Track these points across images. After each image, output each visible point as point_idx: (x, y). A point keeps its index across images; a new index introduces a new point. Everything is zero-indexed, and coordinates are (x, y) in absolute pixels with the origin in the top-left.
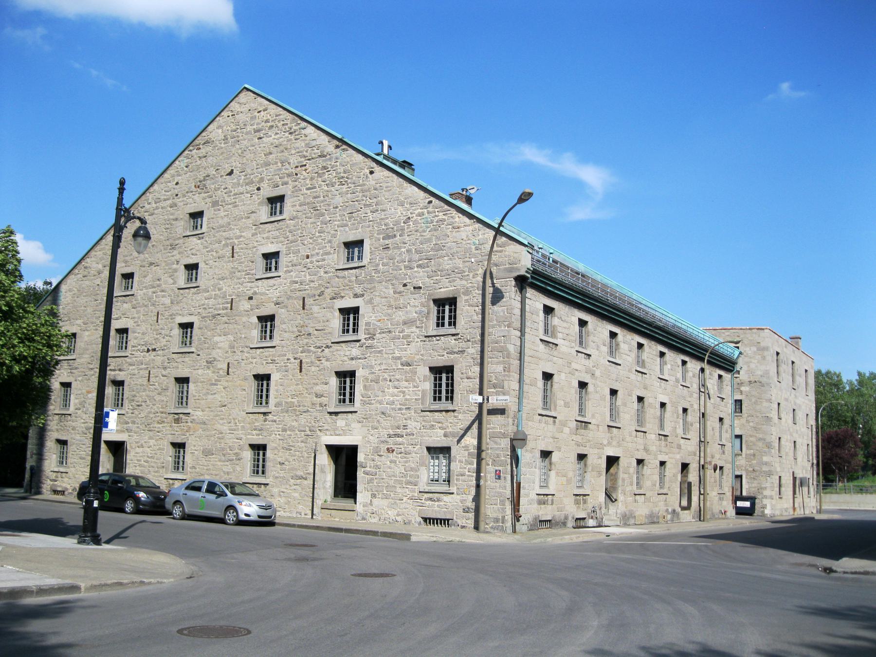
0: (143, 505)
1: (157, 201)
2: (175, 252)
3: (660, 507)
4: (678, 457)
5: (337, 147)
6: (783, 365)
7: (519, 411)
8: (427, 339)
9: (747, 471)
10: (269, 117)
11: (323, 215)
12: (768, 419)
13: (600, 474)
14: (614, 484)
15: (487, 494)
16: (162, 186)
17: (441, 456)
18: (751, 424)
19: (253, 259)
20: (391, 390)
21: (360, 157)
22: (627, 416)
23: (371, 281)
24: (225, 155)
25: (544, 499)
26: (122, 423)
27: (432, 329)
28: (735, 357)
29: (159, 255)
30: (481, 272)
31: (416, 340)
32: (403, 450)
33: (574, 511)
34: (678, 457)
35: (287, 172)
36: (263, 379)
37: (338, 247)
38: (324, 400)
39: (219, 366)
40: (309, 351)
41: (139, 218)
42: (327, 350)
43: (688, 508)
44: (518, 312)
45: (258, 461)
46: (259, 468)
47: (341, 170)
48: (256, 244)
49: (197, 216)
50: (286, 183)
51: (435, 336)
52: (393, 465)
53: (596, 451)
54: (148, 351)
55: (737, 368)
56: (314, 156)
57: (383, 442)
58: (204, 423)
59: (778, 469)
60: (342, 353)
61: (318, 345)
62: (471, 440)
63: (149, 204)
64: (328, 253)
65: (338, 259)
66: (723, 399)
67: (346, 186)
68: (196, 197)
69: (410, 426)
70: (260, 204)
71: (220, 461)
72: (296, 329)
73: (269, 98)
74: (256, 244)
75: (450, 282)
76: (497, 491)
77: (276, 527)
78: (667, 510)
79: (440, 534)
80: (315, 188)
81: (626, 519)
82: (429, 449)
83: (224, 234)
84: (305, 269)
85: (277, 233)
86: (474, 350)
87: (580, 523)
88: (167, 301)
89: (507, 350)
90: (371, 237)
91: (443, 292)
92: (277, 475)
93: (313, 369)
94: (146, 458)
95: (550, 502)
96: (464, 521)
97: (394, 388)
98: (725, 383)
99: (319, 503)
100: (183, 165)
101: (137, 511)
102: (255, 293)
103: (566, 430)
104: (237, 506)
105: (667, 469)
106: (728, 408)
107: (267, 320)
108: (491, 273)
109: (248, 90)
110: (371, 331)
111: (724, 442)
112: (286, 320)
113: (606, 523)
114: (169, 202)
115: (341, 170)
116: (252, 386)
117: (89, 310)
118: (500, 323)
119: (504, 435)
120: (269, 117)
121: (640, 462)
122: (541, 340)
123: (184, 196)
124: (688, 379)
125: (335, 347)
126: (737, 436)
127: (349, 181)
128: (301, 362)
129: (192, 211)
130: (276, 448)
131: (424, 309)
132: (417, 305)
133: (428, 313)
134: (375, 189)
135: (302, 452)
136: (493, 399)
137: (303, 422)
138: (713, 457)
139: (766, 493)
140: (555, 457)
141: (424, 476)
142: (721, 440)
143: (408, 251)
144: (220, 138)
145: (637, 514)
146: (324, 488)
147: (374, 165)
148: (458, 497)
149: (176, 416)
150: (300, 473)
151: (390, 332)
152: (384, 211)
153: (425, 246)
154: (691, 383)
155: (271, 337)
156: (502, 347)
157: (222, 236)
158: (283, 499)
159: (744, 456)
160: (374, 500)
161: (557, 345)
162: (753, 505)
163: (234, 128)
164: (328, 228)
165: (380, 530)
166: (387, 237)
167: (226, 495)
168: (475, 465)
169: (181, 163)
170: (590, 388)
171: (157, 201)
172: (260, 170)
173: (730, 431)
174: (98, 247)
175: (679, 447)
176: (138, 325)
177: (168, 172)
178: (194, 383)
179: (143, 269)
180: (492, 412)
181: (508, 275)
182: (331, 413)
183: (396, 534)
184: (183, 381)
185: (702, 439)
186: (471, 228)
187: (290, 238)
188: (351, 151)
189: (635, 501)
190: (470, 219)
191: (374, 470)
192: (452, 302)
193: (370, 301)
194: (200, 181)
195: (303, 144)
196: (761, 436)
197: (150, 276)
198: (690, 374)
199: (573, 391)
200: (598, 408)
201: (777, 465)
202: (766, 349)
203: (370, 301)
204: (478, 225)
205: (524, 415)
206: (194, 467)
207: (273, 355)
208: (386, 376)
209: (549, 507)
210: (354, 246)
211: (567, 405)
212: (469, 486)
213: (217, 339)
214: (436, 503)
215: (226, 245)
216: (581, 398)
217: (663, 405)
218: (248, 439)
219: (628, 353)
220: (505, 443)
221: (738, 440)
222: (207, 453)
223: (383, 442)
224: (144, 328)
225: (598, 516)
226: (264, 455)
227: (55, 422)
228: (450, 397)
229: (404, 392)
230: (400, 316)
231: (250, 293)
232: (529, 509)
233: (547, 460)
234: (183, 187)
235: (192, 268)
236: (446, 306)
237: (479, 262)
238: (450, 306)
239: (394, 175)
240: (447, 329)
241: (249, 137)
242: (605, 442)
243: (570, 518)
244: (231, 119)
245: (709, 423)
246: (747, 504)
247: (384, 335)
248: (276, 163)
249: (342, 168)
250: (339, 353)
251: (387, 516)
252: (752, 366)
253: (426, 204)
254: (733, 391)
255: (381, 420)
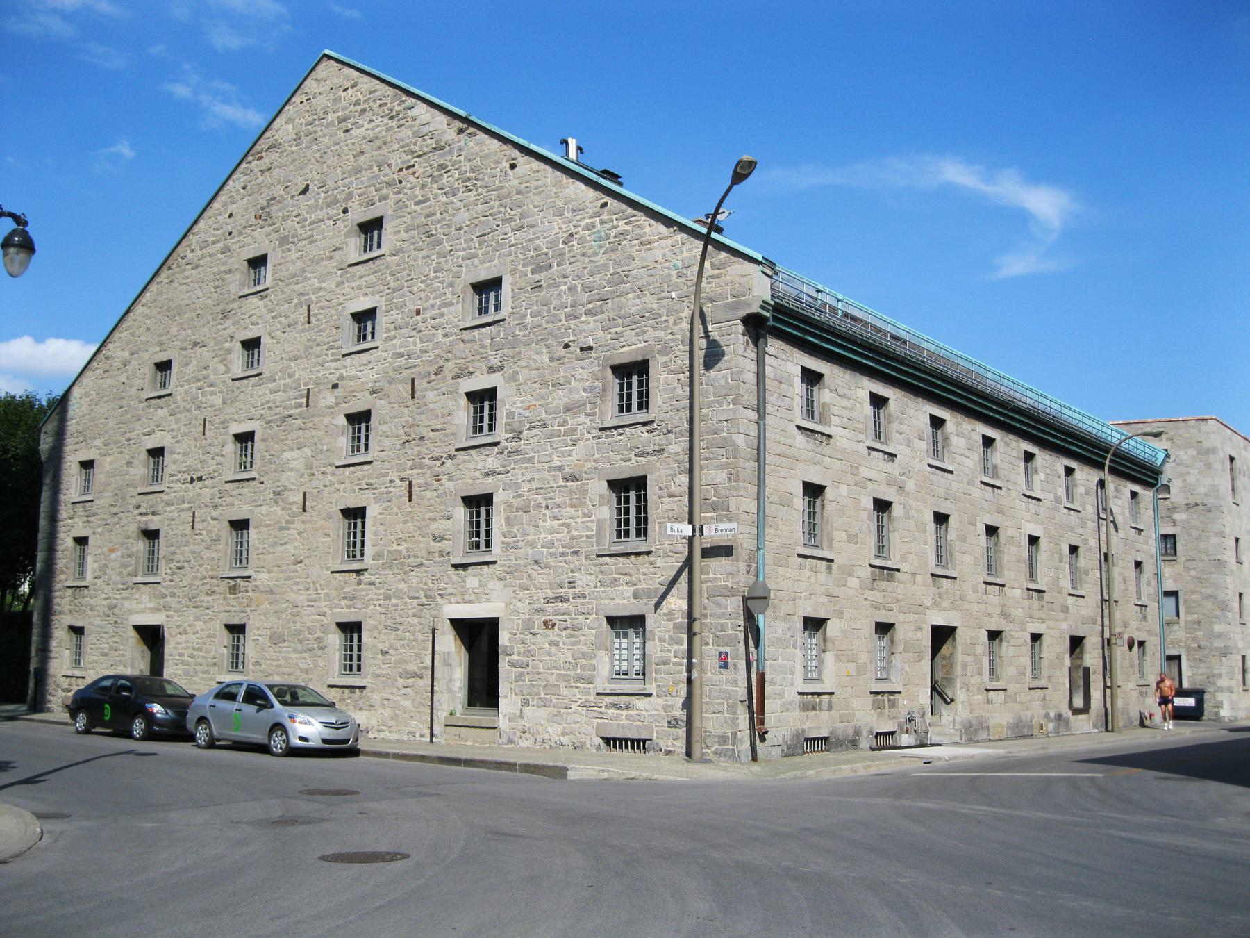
0: (160, 725)
1: (204, 245)
2: (228, 323)
3: (1035, 709)
4: (1064, 625)
5: (461, 131)
6: (1241, 477)
7: (759, 549)
8: (603, 434)
9: (1188, 648)
10: (360, 96)
11: (439, 242)
12: (1220, 564)
13: (919, 655)
14: (948, 673)
15: (706, 696)
16: (210, 222)
17: (631, 631)
18: (1193, 573)
19: (338, 323)
20: (549, 523)
21: (496, 144)
22: (968, 559)
23: (515, 343)
24: (296, 163)
25: (812, 701)
26: (157, 598)
27: (611, 416)
28: (1159, 463)
29: (206, 329)
30: (686, 313)
31: (587, 436)
32: (569, 624)
33: (871, 720)
34: (1064, 625)
35: (386, 179)
36: (355, 515)
37: (464, 292)
38: (445, 545)
39: (292, 499)
40: (422, 466)
41: (12, 215)
42: (449, 463)
43: (1085, 710)
44: (751, 378)
45: (351, 650)
46: (353, 662)
47: (467, 167)
48: (342, 299)
49: (258, 263)
50: (385, 198)
51: (615, 428)
52: (553, 649)
53: (911, 617)
54: (192, 480)
55: (1163, 480)
56: (426, 150)
57: (538, 611)
58: (271, 592)
59: (1240, 644)
60: (472, 466)
61: (435, 454)
62: (677, 602)
63: (193, 251)
64: (448, 304)
65: (464, 310)
66: (1140, 531)
67: (474, 193)
68: (256, 234)
69: (579, 582)
70: (348, 235)
71: (295, 651)
72: (402, 432)
73: (360, 66)
74: (342, 299)
75: (637, 335)
76: (723, 688)
77: (362, 758)
78: (1047, 716)
79: (627, 766)
80: (428, 200)
81: (971, 733)
82: (611, 620)
83: (296, 287)
84: (414, 333)
85: (372, 279)
86: (677, 447)
87: (884, 740)
88: (218, 400)
89: (734, 444)
90: (512, 272)
91: (627, 353)
92: (378, 672)
93: (429, 494)
94: (191, 651)
95: (825, 706)
96: (670, 742)
97: (556, 520)
98: (1142, 505)
99: (441, 716)
100: (239, 186)
101: (150, 736)
102: (342, 378)
103: (853, 582)
104: (288, 723)
105: (1044, 647)
106: (1149, 547)
107: (359, 419)
108: (702, 315)
109: (330, 57)
110: (516, 426)
111: (1144, 601)
112: (387, 418)
113: (933, 738)
114: (219, 246)
115: (467, 167)
116: (340, 526)
117: (112, 423)
118: (720, 398)
119: (731, 592)
120: (360, 96)
121: (994, 635)
122: (799, 428)
123: (240, 234)
124: (1077, 496)
125: (462, 456)
126: (1167, 594)
127: (479, 184)
128: (410, 483)
129: (251, 256)
130: (376, 627)
131: (597, 383)
132: (588, 379)
133: (604, 390)
134: (519, 193)
135: (414, 633)
136: (709, 530)
137: (415, 582)
138: (1126, 625)
139: (1222, 682)
140: (832, 628)
141: (603, 667)
142: (1139, 598)
143: (570, 289)
144: (289, 138)
145: (992, 722)
146: (450, 691)
147: (516, 153)
148: (660, 701)
149: (232, 582)
150: (412, 667)
151: (544, 426)
152: (532, 226)
153: (597, 278)
154: (1083, 504)
155: (366, 449)
156: (724, 439)
157: (293, 291)
158: (388, 710)
159: (1182, 624)
160: (526, 709)
161: (830, 436)
162: (1200, 702)
163: (310, 119)
164: (449, 263)
165: (519, 761)
166: (538, 269)
167: (272, 706)
168: (685, 646)
169: (234, 185)
170: (897, 510)
171: (204, 245)
172: (346, 181)
173: (1153, 582)
174: (124, 325)
175: (1065, 609)
176: (177, 442)
177: (218, 199)
178: (257, 527)
179: (184, 353)
180: (708, 553)
181: (730, 315)
182: (456, 566)
183: (544, 767)
184: (240, 525)
185: (1106, 597)
186: (669, 241)
187: (392, 285)
188: (481, 136)
189: (988, 701)
190: (668, 226)
191: (525, 659)
192: (641, 368)
193: (513, 378)
194: (263, 209)
195: (410, 133)
196: (1209, 591)
197: (194, 362)
198: (1081, 490)
199: (864, 515)
200: (912, 543)
201: (1238, 637)
202: (1211, 451)
203: (513, 378)
204: (681, 236)
205: (769, 558)
206: (257, 663)
207: (369, 476)
208: (540, 499)
209: (824, 715)
210: (487, 288)
211: (852, 539)
212: (676, 682)
213: (288, 455)
214: (625, 713)
215: (300, 305)
216: (880, 528)
217: (1033, 540)
218: (334, 614)
219: (967, 453)
220: (734, 605)
221: (1172, 600)
222: (277, 639)
223: (538, 611)
224: (185, 446)
225: (918, 727)
226: (360, 639)
227: (67, 599)
228: (642, 532)
229: (568, 526)
230: (560, 398)
231: (334, 379)
232: (784, 718)
233: (819, 634)
234: (239, 220)
235: (252, 345)
236: (632, 373)
237: (683, 298)
238: (640, 376)
239: (548, 167)
240: (637, 416)
241: (331, 130)
242: (928, 602)
243: (865, 733)
244: (306, 106)
245: (1116, 572)
246: (1190, 702)
247: (535, 432)
248: (371, 167)
249: (468, 165)
250: (467, 465)
251: (546, 736)
252: (1191, 479)
253: (598, 209)
254: (1157, 517)
255: (534, 574)
